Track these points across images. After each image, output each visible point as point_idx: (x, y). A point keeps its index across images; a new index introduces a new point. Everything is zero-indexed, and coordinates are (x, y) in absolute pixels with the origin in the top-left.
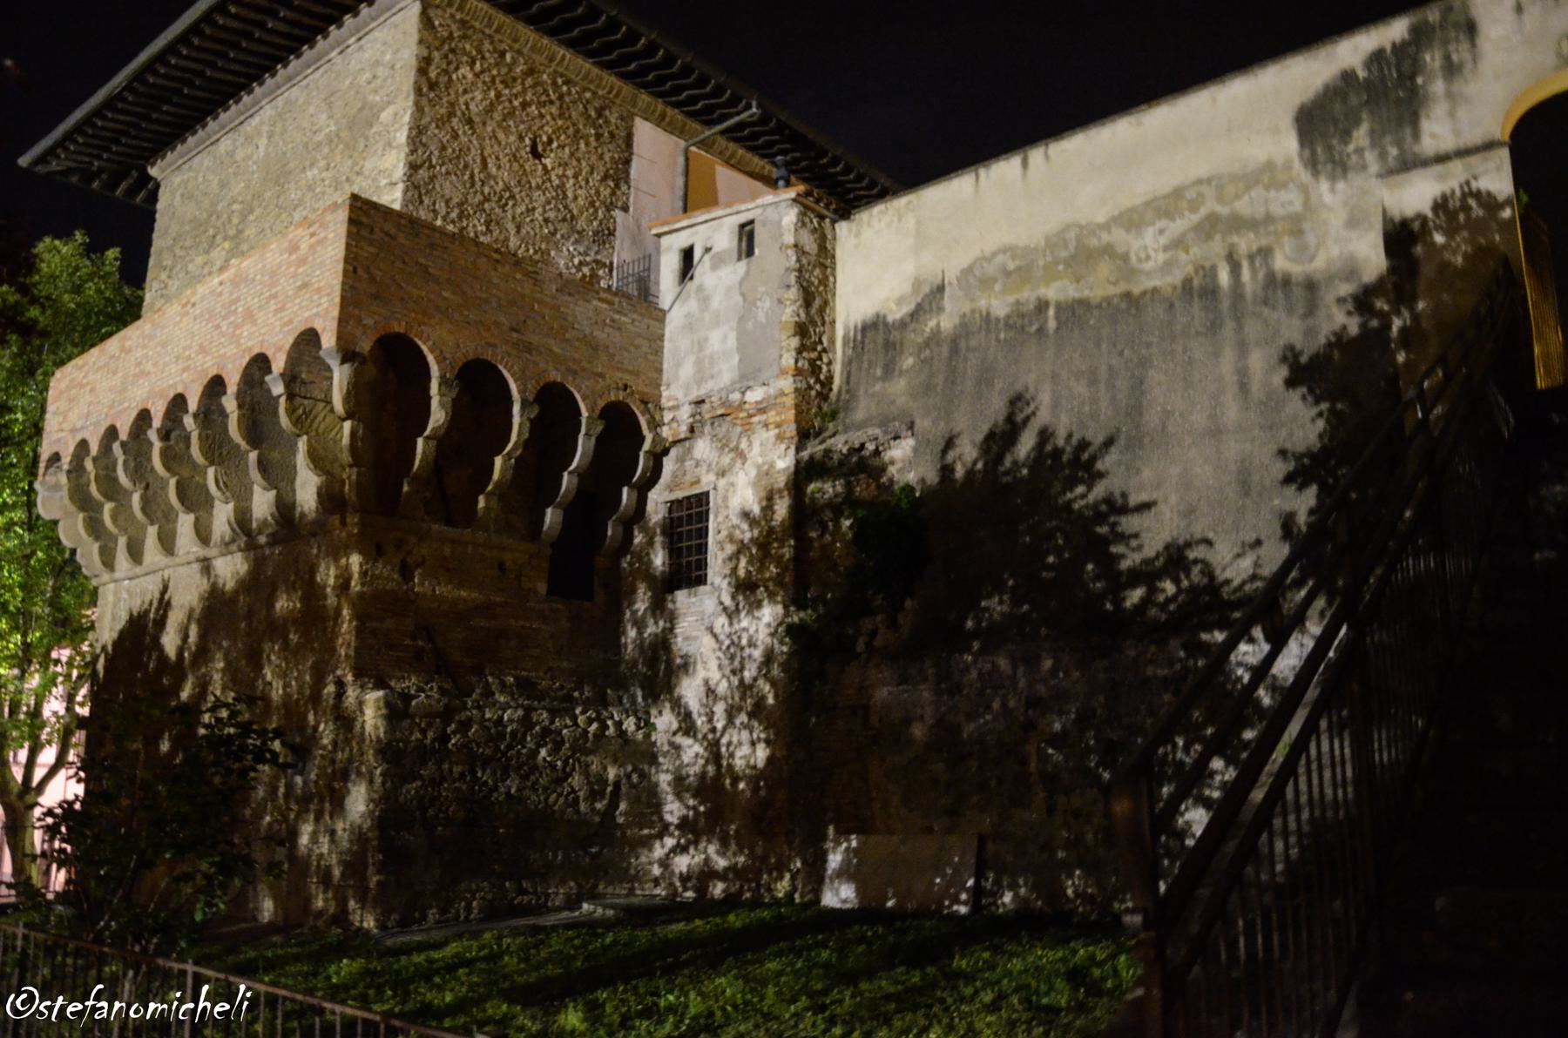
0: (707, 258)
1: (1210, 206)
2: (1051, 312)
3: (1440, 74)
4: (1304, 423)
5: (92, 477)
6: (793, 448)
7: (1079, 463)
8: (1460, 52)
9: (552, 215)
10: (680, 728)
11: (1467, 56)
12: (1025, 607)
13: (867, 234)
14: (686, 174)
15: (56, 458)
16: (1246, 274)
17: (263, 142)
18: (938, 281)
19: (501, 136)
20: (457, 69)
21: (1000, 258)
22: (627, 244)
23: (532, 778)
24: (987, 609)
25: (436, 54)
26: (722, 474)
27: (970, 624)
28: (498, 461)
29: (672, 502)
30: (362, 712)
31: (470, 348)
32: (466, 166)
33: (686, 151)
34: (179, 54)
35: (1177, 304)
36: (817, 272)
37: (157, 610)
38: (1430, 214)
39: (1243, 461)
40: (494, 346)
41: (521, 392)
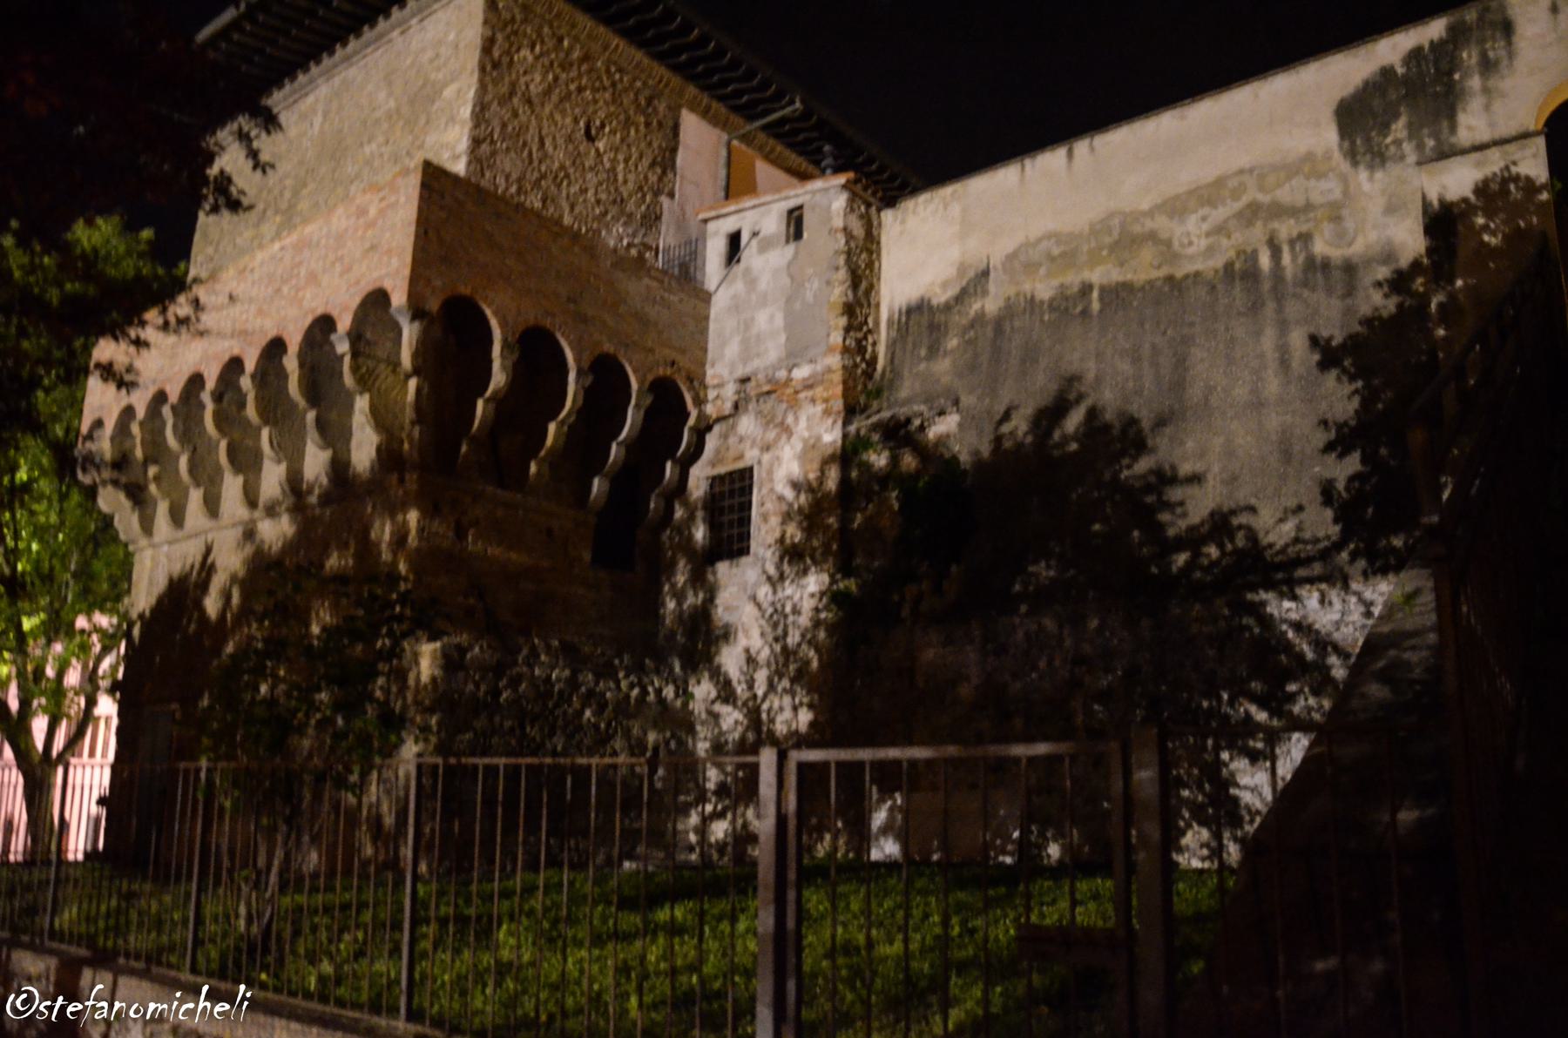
0: (754, 242)
1: (1252, 194)
2: (1095, 294)
3: (1476, 69)
4: (1340, 398)
5: (138, 441)
6: (840, 423)
7: (1128, 437)
8: (1496, 50)
9: (603, 196)
10: (719, 697)
11: (1503, 53)
12: (1072, 572)
13: (912, 222)
14: (729, 164)
15: (99, 424)
16: (1286, 259)
17: (318, 120)
18: (983, 266)
19: (558, 117)
20: (518, 50)
21: (1044, 244)
22: (672, 231)
23: (577, 737)
24: (1033, 574)
25: (499, 37)
26: (767, 448)
27: (1017, 587)
28: (552, 427)
29: (714, 479)
30: (417, 663)
31: (531, 315)
32: (525, 144)
33: (729, 144)
34: (242, 31)
35: (1220, 287)
36: (864, 256)
37: (199, 574)
38: (1472, 198)
39: (1284, 432)
40: (553, 315)
41: (578, 360)
